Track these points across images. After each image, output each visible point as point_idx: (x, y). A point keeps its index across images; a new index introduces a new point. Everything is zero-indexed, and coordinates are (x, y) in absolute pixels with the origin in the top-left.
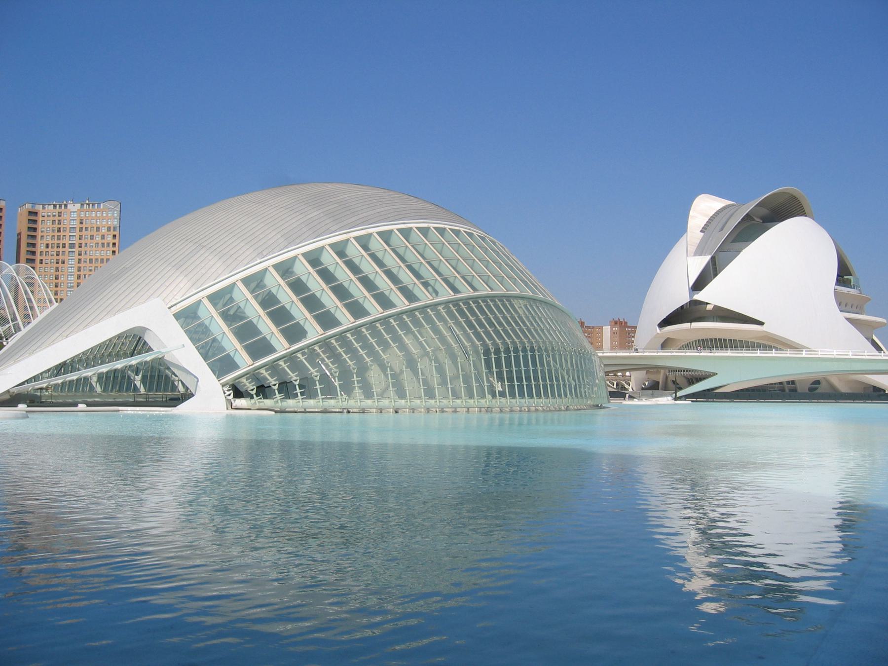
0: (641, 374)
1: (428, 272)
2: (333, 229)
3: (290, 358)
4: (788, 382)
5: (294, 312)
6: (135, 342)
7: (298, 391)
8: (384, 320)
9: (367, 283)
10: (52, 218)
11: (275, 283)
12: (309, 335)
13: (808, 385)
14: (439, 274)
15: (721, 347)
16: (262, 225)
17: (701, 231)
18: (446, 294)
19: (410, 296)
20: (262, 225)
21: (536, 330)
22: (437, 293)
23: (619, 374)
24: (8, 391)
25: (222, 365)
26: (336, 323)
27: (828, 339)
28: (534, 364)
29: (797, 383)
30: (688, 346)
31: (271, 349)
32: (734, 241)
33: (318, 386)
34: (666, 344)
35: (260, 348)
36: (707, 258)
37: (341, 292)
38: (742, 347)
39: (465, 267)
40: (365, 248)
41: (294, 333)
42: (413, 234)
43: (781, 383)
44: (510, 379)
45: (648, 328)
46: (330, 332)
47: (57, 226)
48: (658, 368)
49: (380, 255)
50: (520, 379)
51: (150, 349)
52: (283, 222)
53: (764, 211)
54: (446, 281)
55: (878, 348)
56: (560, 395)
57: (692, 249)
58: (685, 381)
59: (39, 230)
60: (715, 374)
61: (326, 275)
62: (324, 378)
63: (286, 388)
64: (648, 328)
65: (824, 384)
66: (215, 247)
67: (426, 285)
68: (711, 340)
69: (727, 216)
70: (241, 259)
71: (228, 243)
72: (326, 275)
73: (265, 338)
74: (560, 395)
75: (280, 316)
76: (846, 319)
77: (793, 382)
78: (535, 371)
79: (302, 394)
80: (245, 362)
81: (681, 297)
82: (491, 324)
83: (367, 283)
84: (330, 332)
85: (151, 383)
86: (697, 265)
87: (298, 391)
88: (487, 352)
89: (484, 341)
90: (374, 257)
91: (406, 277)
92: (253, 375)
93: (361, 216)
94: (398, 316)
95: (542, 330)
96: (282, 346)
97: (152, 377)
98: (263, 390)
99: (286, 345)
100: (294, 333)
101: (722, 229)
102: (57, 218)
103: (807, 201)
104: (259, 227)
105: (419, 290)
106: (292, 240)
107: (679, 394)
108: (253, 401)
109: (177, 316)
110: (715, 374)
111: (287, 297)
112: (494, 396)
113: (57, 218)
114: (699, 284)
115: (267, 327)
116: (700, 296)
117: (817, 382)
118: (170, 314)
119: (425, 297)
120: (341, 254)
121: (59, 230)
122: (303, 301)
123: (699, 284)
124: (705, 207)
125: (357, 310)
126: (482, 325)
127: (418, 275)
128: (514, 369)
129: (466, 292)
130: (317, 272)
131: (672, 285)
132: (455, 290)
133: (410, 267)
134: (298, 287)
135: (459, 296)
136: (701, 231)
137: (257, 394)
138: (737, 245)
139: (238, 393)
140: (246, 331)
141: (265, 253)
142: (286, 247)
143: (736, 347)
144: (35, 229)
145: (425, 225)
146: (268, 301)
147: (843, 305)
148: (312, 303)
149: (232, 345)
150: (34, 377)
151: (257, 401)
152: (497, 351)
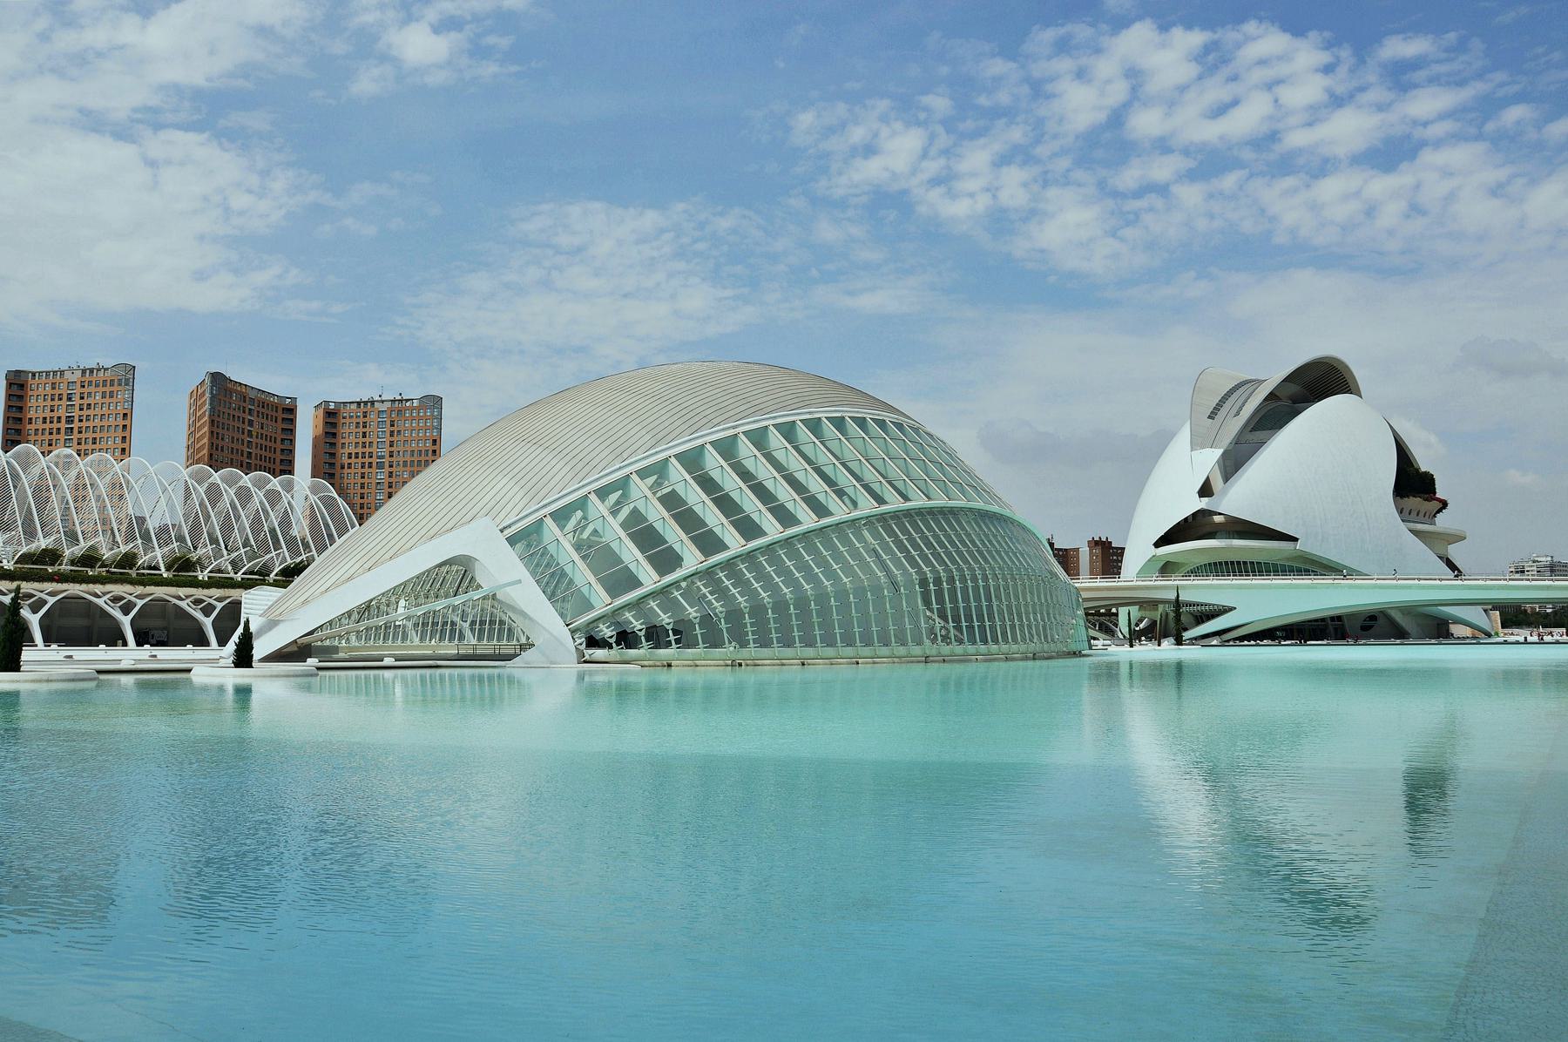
1: (844, 479)
3: (662, 593)
4: (1332, 618)
6: (459, 572)
7: (672, 638)
8: (749, 557)
9: (761, 491)
10: (354, 420)
16: (562, 463)
18: (867, 506)
19: (820, 510)
21: (989, 552)
22: (855, 504)
24: (295, 641)
26: (720, 546)
28: (991, 618)
30: (1196, 572)
31: (635, 583)
32: (1253, 430)
33: (698, 631)
34: (1167, 568)
35: (622, 580)
36: (1221, 451)
37: (725, 504)
38: (1268, 572)
39: (894, 471)
41: (665, 560)
43: (1323, 620)
44: (956, 619)
46: (668, 579)
47: (361, 430)
48: (1154, 604)
50: (969, 618)
51: (479, 587)
53: (1294, 388)
54: (867, 487)
56: (1024, 640)
58: (1192, 619)
59: (339, 436)
61: (708, 484)
62: (706, 620)
63: (656, 636)
64: (1139, 552)
65: (1381, 621)
67: (840, 493)
70: (594, 463)
72: (708, 484)
74: (1024, 640)
75: (688, 519)
76: (1415, 533)
78: (990, 607)
79: (677, 641)
80: (601, 602)
82: (929, 545)
83: (761, 491)
84: (668, 579)
85: (481, 631)
87: (672, 638)
88: (924, 583)
89: (905, 569)
91: (816, 485)
92: (612, 617)
94: (769, 549)
95: (998, 552)
96: (649, 578)
97: (482, 623)
98: (626, 638)
99: (656, 577)
100: (665, 560)
101: (1238, 414)
102: (361, 420)
103: (1360, 374)
105: (833, 503)
107: (1187, 635)
108: (612, 652)
109: (512, 541)
112: (934, 641)
113: (361, 420)
115: (631, 555)
118: (502, 538)
119: (840, 512)
121: (364, 435)
122: (715, 501)
123: (1206, 490)
125: (749, 529)
126: (916, 546)
128: (948, 606)
129: (895, 503)
132: (880, 500)
135: (884, 508)
137: (618, 643)
138: (1260, 435)
139: (593, 642)
140: (646, 537)
141: (625, 455)
143: (1261, 573)
144: (334, 435)
146: (672, 501)
147: (1406, 512)
149: (583, 576)
150: (330, 622)
151: (615, 653)
152: (938, 581)
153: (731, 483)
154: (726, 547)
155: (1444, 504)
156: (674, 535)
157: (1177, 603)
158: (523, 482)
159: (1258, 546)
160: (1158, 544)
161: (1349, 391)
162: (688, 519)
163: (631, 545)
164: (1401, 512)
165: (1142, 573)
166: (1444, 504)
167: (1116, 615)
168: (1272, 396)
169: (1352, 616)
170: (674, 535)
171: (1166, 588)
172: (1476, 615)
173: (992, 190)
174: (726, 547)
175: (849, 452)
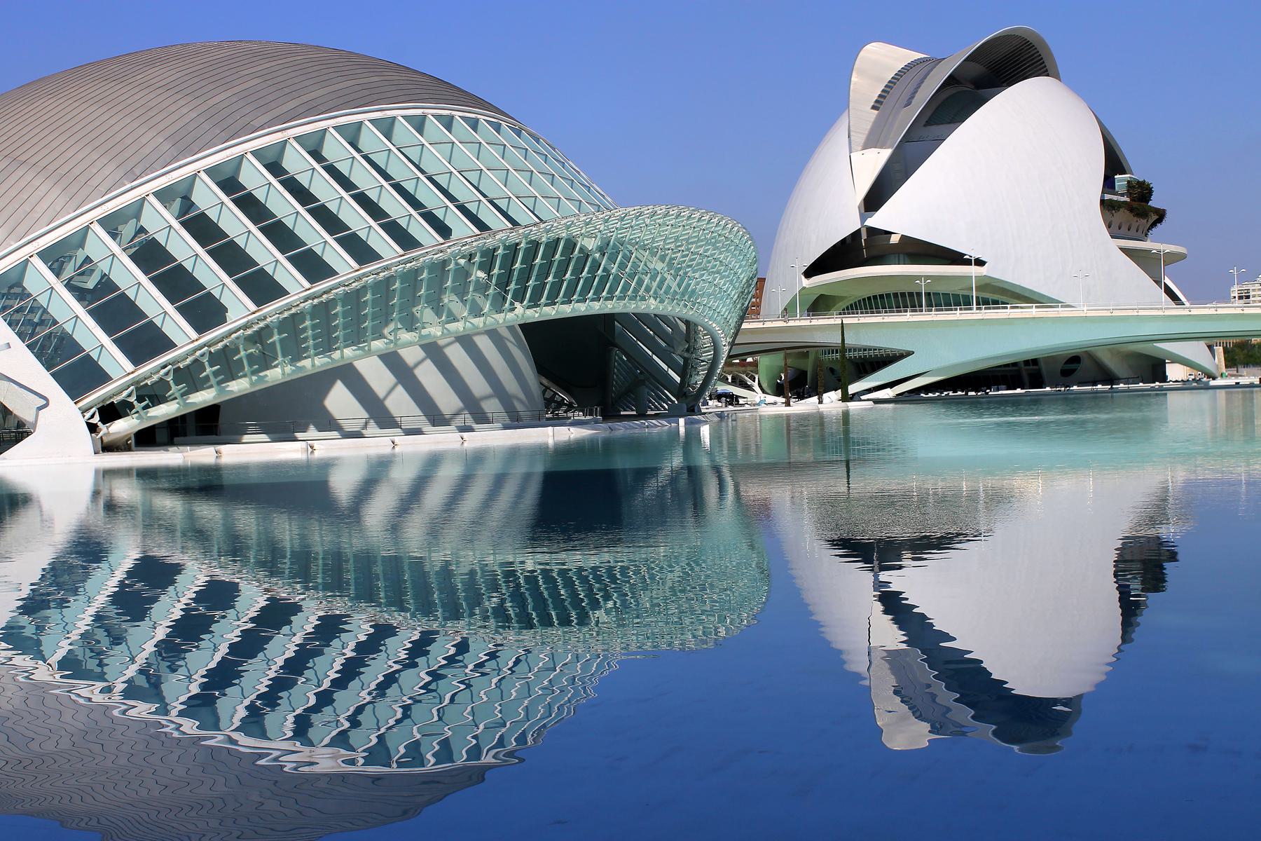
0: (776, 360)
2: (256, 123)
4: (1027, 362)
5: (201, 274)
11: (162, 223)
12: (230, 316)
13: (1060, 366)
14: (451, 198)
15: (913, 306)
16: (128, 120)
17: (874, 108)
20: (135, 124)
23: (750, 360)
25: (78, 375)
27: (1090, 289)
29: (1042, 364)
30: (854, 308)
34: (820, 304)
36: (886, 154)
37: (280, 235)
39: (493, 184)
40: (317, 155)
41: (205, 313)
42: (397, 130)
43: (1015, 364)
45: (788, 280)
49: (343, 168)
52: (164, 114)
53: (977, 69)
54: (463, 209)
55: (1174, 297)
57: (860, 138)
60: (909, 353)
61: (251, 206)
66: (77, 171)
68: (896, 295)
69: (917, 80)
70: (94, 182)
71: (54, 145)
72: (251, 206)
73: (151, 323)
75: (176, 283)
76: (1124, 250)
77: (1035, 362)
81: (844, 220)
86: (873, 162)
90: (332, 171)
93: (305, 98)
101: (908, 104)
103: (1057, 46)
104: (121, 124)
106: (185, 146)
107: (853, 389)
110: (909, 353)
111: (184, 248)
114: (874, 201)
116: (878, 220)
117: (1075, 359)
120: (275, 168)
123: (874, 201)
124: (881, 60)
127: (346, 183)
130: (235, 201)
131: (831, 200)
133: (398, 188)
134: (202, 228)
136: (874, 108)
138: (936, 130)
140: (114, 310)
141: (137, 171)
142: (175, 159)
145: (419, 112)
146: (149, 255)
148: (231, 257)
149: (93, 337)
153: (282, 205)
154: (170, 345)
155: (1161, 215)
156: (153, 303)
157: (843, 348)
158: (120, 159)
159: (933, 272)
160: (809, 273)
161: (1045, 73)
162: (176, 283)
163: (90, 322)
164: (1109, 226)
165: (788, 312)
166: (1161, 215)
167: (755, 364)
168: (952, 80)
169: (1051, 359)
170: (153, 303)
171: (824, 329)
172: (1196, 352)
173: (846, 398)
174: (170, 345)
175: (435, 160)
